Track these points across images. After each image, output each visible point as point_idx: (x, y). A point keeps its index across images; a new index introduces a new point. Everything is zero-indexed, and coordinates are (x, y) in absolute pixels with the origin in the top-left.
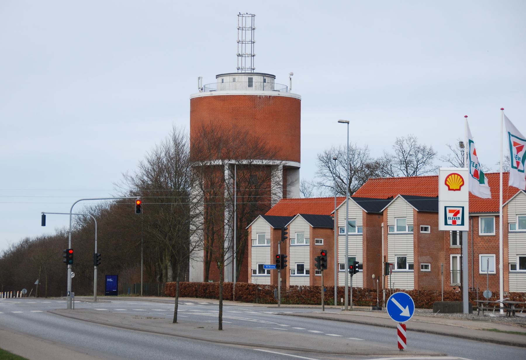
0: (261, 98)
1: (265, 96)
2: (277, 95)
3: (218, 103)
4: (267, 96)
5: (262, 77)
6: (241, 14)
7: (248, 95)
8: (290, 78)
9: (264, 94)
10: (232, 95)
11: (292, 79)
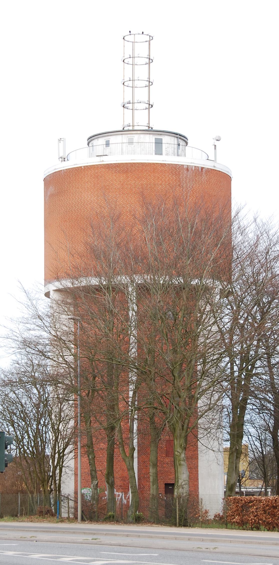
0: (190, 170)
1: (195, 167)
2: (211, 166)
3: (115, 176)
4: (198, 167)
5: (176, 139)
6: (131, 33)
7: (168, 164)
8: (214, 146)
9: (194, 163)
10: (141, 163)
11: (217, 147)
